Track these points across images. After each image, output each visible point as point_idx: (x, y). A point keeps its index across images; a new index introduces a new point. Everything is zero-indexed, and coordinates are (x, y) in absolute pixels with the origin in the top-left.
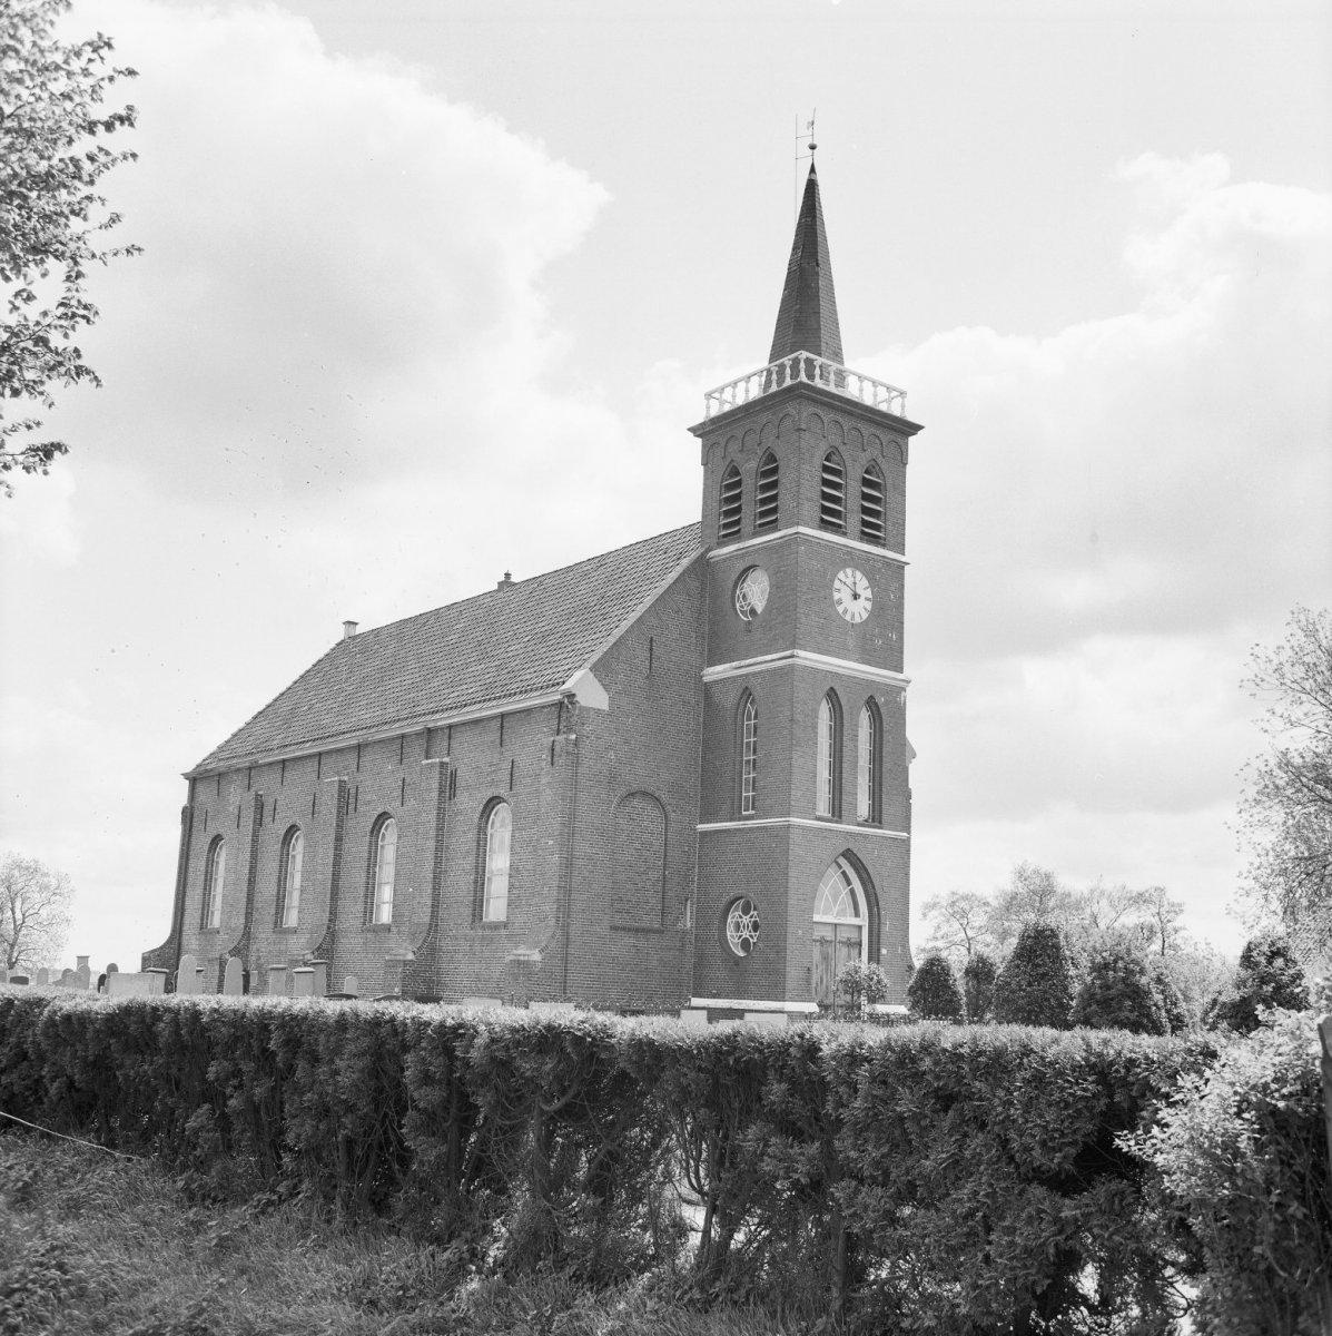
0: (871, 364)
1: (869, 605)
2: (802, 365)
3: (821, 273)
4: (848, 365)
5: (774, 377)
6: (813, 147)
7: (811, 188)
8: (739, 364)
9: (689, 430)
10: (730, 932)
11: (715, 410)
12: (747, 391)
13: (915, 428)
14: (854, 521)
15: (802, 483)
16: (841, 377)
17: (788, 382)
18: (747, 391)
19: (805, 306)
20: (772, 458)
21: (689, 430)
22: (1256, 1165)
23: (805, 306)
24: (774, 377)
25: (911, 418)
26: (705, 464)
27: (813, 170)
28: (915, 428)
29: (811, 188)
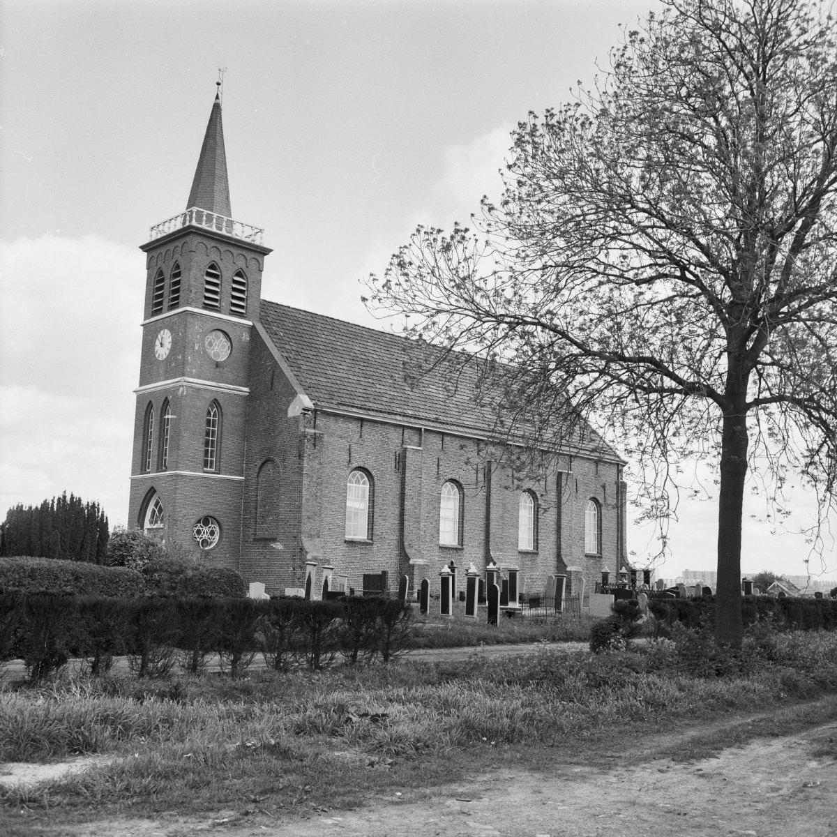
0: (246, 215)
1: (167, 352)
2: (194, 215)
3: (219, 159)
4: (235, 216)
5: (188, 218)
6: (218, 84)
7: (217, 108)
8: (168, 207)
9: (142, 247)
10: (217, 538)
11: (156, 236)
12: (175, 225)
13: (264, 252)
14: (226, 301)
15: (194, 278)
16: (230, 224)
17: (187, 224)
18: (175, 225)
19: (209, 175)
20: (178, 267)
21: (142, 247)
22: (714, 593)
23: (209, 175)
24: (188, 218)
25: (266, 245)
26: (148, 269)
27: (217, 97)
28: (264, 252)
29: (217, 108)
